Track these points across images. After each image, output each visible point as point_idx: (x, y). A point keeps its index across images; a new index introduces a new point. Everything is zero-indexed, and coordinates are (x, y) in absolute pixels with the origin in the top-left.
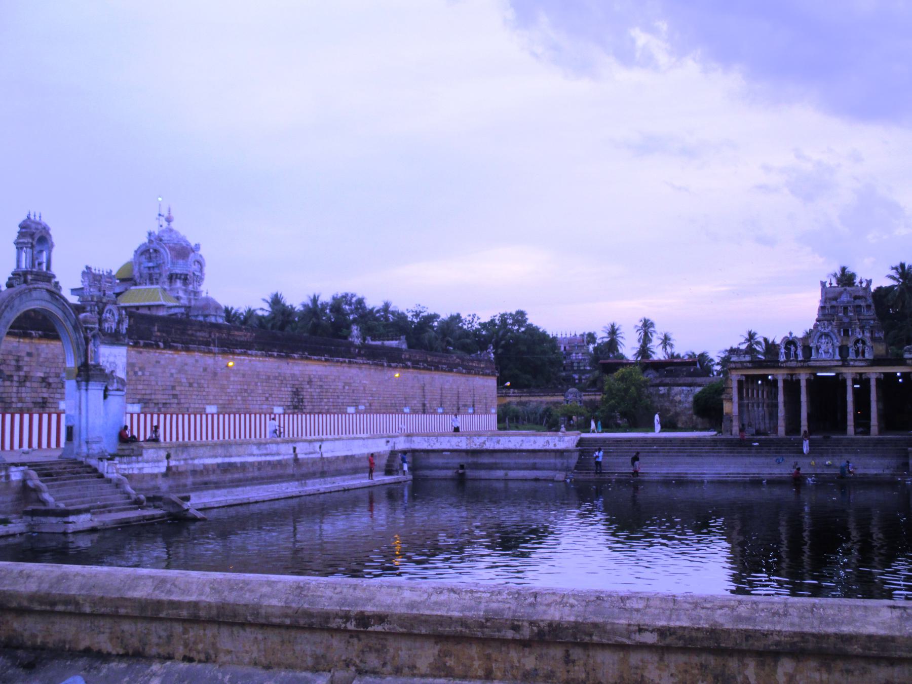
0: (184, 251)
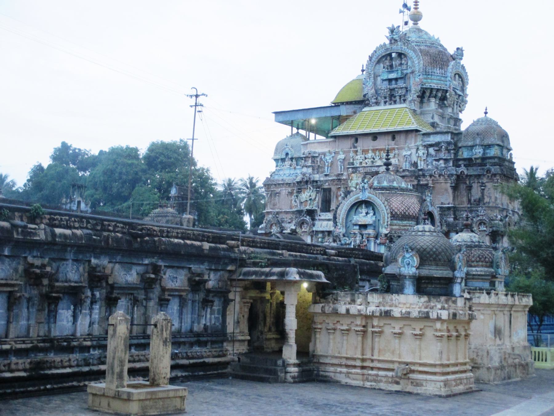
0: (439, 58)
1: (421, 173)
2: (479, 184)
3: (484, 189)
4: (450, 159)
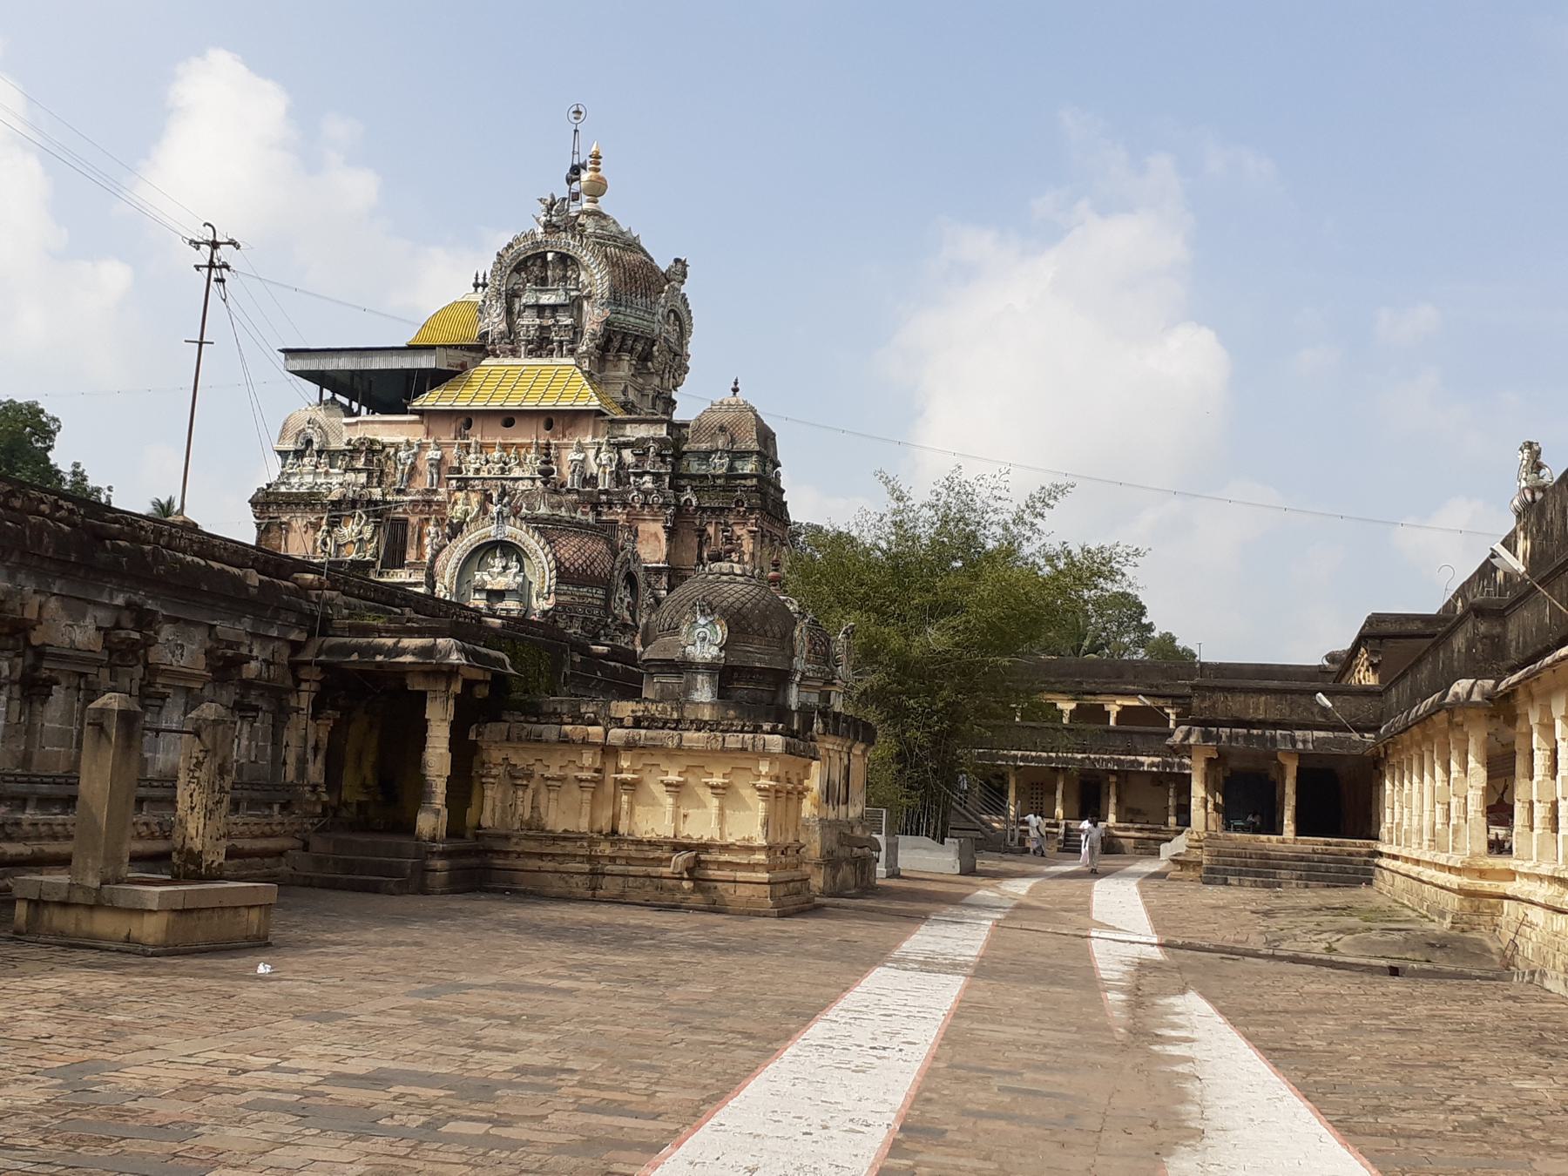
0: (642, 280)
1: (604, 497)
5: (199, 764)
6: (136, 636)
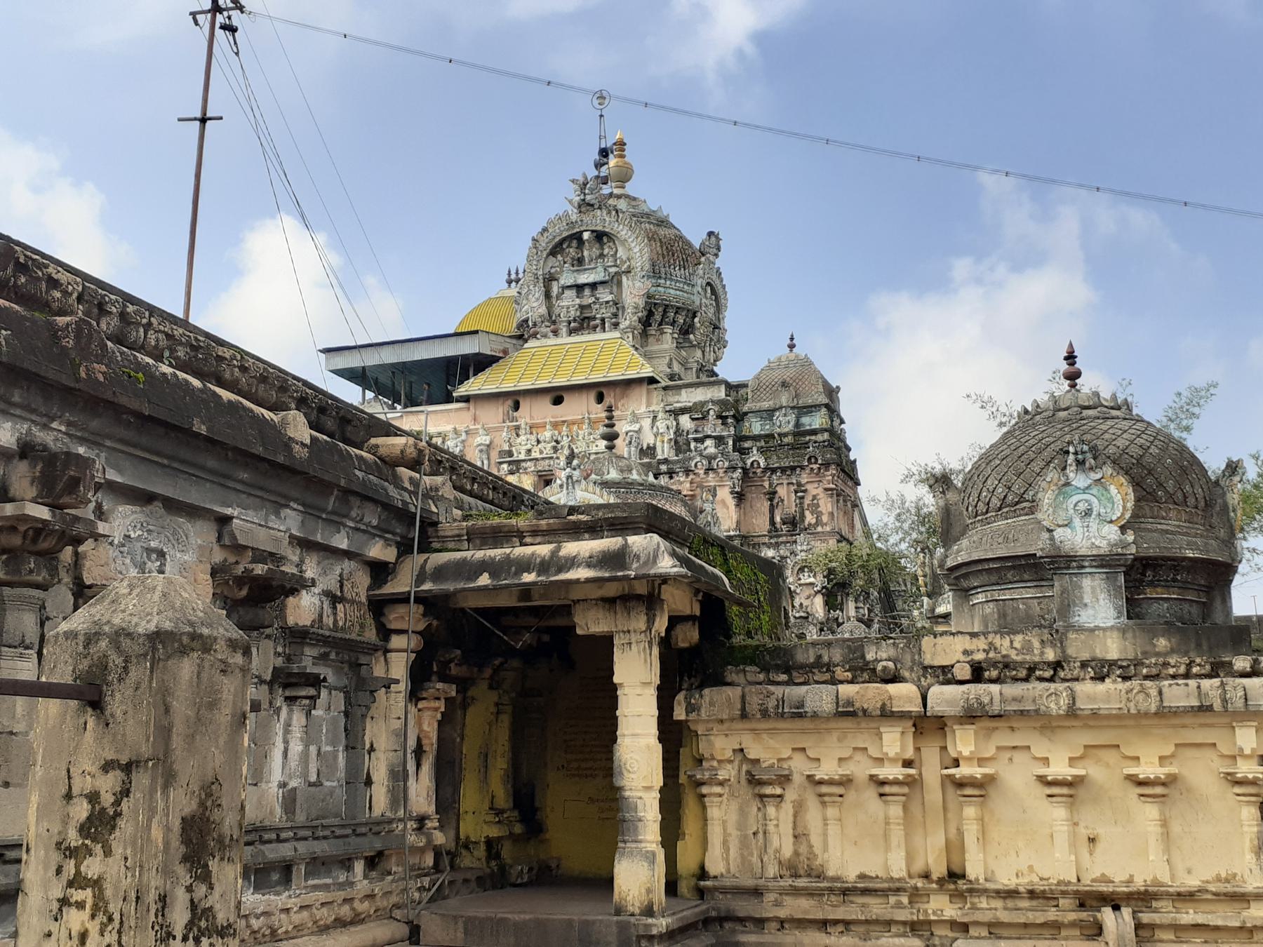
2: (792, 488)
3: (802, 498)
4: (729, 436)
5: (100, 825)
6: (43, 513)
